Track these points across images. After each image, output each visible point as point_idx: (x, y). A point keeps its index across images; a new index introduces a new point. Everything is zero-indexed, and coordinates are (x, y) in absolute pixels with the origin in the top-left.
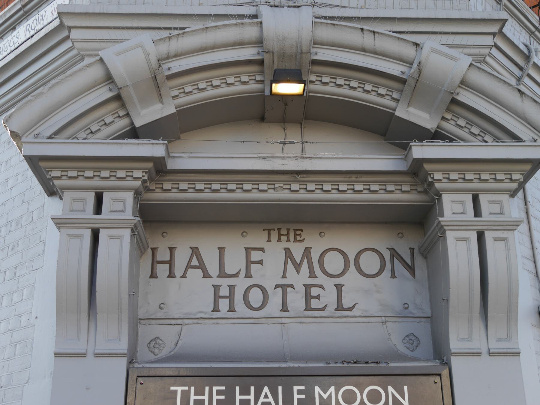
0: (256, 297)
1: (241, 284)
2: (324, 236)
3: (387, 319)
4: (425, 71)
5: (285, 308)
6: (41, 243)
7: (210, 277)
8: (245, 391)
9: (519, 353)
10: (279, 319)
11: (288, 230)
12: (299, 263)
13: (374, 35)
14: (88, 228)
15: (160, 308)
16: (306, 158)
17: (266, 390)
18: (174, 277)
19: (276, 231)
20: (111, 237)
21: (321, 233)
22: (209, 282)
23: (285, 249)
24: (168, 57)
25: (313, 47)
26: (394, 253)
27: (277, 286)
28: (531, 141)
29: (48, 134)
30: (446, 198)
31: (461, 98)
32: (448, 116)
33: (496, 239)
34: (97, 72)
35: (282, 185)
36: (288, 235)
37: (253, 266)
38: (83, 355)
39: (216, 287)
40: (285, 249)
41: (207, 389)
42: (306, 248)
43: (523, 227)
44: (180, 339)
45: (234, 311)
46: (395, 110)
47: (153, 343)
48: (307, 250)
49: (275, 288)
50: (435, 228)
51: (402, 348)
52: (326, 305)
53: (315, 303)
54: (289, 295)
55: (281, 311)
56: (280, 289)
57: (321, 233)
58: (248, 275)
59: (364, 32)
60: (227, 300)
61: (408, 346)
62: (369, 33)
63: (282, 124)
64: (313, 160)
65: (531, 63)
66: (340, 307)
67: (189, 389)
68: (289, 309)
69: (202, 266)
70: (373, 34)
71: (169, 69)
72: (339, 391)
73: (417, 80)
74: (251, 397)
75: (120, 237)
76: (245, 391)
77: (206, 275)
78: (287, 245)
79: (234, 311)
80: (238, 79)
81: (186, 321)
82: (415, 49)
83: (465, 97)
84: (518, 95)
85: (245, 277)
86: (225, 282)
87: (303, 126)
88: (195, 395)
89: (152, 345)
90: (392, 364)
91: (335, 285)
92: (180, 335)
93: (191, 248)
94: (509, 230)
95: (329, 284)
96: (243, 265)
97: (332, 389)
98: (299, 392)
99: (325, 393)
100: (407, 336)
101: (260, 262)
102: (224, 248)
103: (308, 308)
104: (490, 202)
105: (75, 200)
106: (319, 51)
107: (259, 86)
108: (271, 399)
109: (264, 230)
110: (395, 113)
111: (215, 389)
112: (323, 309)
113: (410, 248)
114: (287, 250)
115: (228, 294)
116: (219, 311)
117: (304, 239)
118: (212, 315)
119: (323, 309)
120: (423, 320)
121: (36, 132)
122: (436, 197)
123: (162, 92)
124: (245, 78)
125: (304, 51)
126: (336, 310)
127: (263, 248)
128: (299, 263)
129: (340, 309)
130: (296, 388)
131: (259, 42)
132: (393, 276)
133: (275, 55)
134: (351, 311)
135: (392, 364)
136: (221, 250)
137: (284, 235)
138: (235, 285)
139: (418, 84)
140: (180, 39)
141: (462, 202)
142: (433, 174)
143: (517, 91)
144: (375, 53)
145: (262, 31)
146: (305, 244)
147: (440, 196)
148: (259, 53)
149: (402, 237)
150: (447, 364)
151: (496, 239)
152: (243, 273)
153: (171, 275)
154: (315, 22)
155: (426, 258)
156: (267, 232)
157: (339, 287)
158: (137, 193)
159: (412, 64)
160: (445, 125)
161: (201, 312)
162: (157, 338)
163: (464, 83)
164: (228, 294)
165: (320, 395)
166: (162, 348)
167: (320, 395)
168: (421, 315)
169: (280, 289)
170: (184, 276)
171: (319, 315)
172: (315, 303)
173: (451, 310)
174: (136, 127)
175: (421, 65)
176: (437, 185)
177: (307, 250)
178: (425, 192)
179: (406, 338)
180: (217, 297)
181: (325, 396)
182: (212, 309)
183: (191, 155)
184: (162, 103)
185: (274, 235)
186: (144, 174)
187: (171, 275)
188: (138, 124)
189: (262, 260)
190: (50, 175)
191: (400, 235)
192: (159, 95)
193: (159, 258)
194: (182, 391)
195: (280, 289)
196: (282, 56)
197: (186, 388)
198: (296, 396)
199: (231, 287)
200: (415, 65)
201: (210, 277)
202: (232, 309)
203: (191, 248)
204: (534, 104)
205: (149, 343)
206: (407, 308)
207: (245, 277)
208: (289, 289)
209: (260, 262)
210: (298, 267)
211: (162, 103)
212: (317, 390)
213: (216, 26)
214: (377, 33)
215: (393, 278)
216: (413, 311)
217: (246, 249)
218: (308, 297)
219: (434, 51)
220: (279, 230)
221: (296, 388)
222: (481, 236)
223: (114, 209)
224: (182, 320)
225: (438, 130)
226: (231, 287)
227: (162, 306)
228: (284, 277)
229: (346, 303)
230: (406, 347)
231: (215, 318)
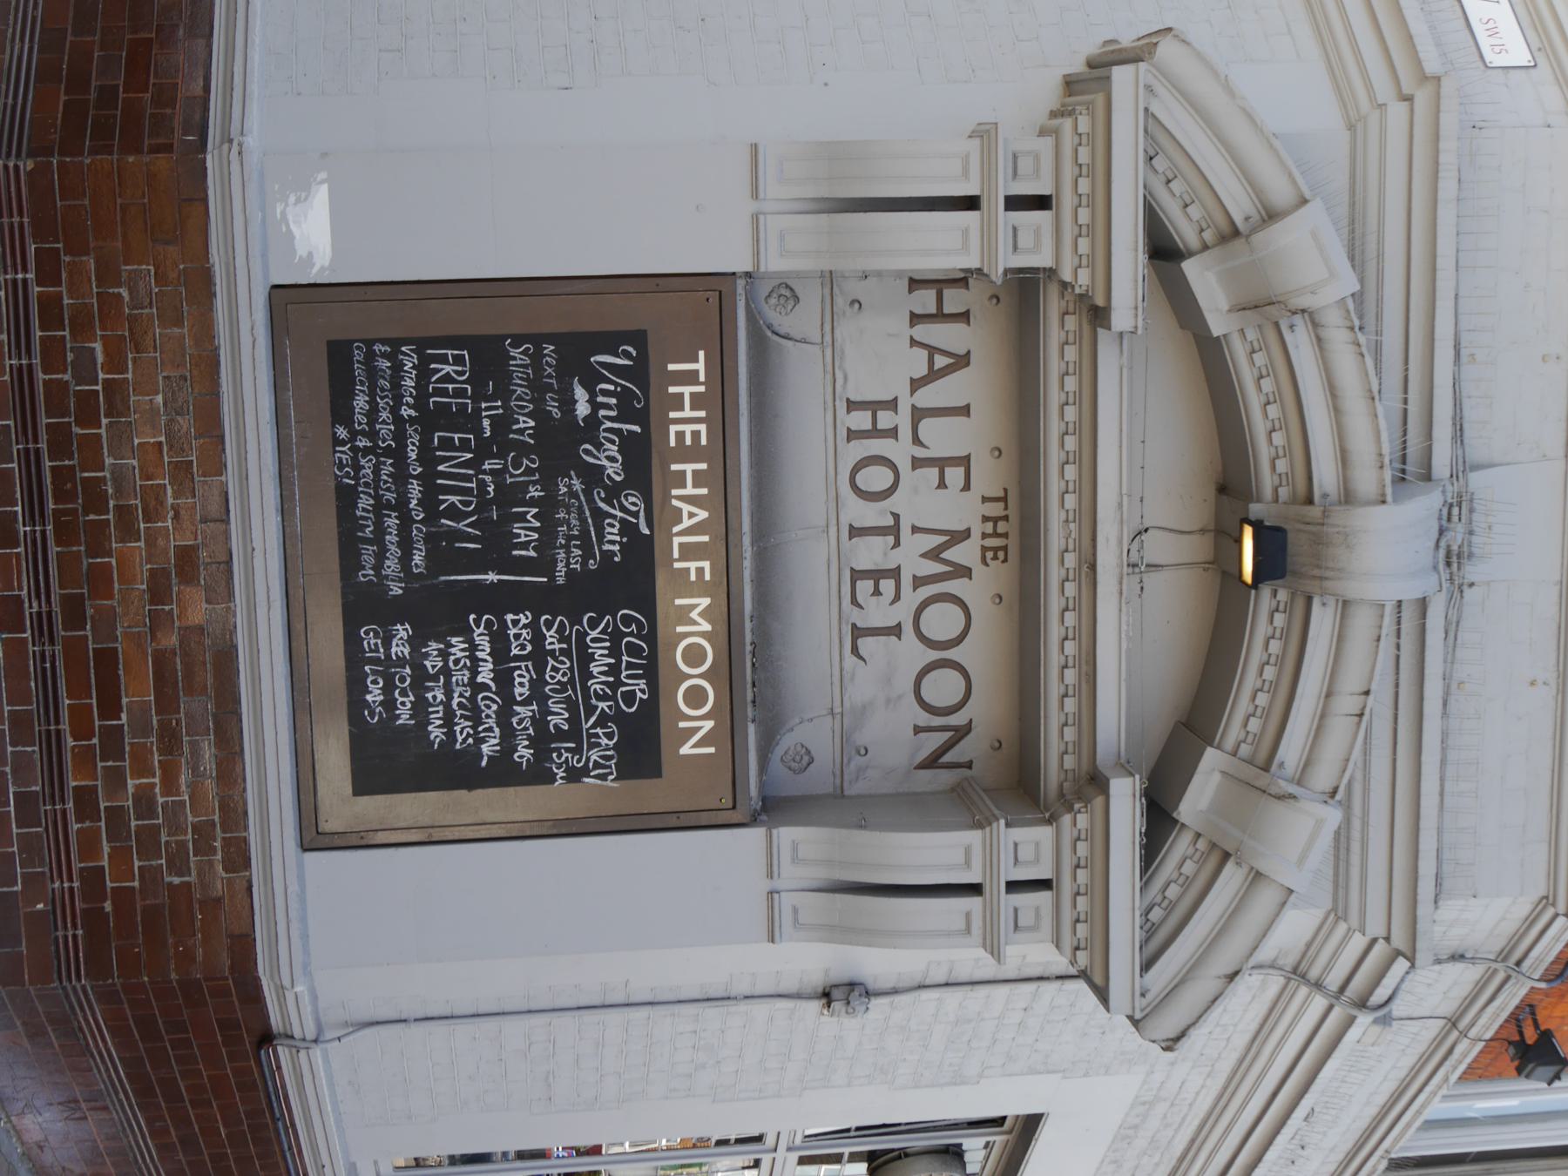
0: (876, 478)
1: (900, 451)
2: (994, 603)
4: (1279, 808)
5: (855, 532)
6: (970, 71)
7: (913, 392)
8: (699, 479)
9: (773, 941)
10: (834, 522)
11: (1005, 535)
12: (941, 556)
13: (1356, 715)
14: (983, 190)
15: (852, 302)
16: (1121, 583)
17: (703, 515)
18: (912, 325)
19: (1003, 513)
20: (966, 232)
21: (1001, 598)
22: (902, 391)
23: (968, 531)
24: (1315, 325)
25: (1337, 600)
26: (962, 732)
27: (896, 517)
28: (1141, 987)
30: (1044, 833)
31: (1230, 867)
32: (1201, 845)
33: (968, 915)
34: (1280, 193)
35: (1073, 536)
36: (996, 534)
37: (936, 471)
38: (755, 194)
39: (892, 405)
40: (968, 531)
41: (702, 414)
42: (970, 570)
43: (988, 968)
44: (797, 344)
45: (849, 440)
46: (1218, 748)
47: (788, 293)
48: (964, 572)
49: (892, 513)
50: (990, 810)
51: (787, 742)
52: (861, 607)
53: (865, 586)
54: (879, 539)
55: (851, 525)
56: (892, 523)
57: (1001, 598)
58: (917, 463)
59: (1363, 697)
60: (868, 426)
61: (791, 753)
62: (1361, 707)
64: (1117, 595)
65: (1354, 1012)
66: (858, 632)
67: (701, 384)
68: (854, 540)
69: (933, 375)
70: (1359, 712)
72: (705, 638)
73: (1264, 792)
74: (690, 490)
76: (699, 479)
77: (916, 384)
79: (849, 440)
80: (1281, 453)
82: (1327, 791)
83: (1232, 878)
85: (913, 457)
86: (903, 420)
87: (1207, 566)
88: (691, 394)
89: (784, 291)
90: (751, 728)
91: (899, 624)
93: (969, 352)
94: (985, 939)
95: (902, 613)
97: (706, 627)
98: (700, 571)
99: (700, 614)
100: (808, 752)
101: (942, 484)
102: (968, 415)
103: (857, 575)
105: (1037, 158)
107: (1268, 492)
108: (687, 523)
109: (1005, 490)
110: (1212, 746)
111: (702, 428)
112: (854, 601)
113: (971, 762)
114: (967, 534)
117: (987, 565)
118: (841, 400)
119: (854, 601)
120: (838, 781)
121: (1159, 88)
122: (1047, 815)
123: (1248, 312)
124: (1282, 466)
125: (1328, 584)
126: (854, 626)
127: (969, 489)
128: (941, 556)
129: (855, 632)
130: (706, 565)
131: (1348, 497)
132: (918, 730)
133: (1319, 527)
134: (852, 652)
135: (751, 728)
136: (965, 411)
137: (995, 527)
138: (897, 439)
139: (1259, 792)
140: (1352, 348)
141: (1037, 860)
142: (1087, 812)
143: (1237, 969)
144: (1323, 716)
145: (1369, 503)
146: (978, 569)
147: (1049, 822)
148: (1325, 496)
149: (993, 748)
150: (752, 821)
151: (968, 915)
152: (920, 453)
153: (915, 318)
154: (1384, 605)
155: (953, 790)
156: (1001, 494)
157: (896, 631)
158: (1051, 273)
159: (1299, 783)
162: (797, 299)
166: (778, 310)
168: (846, 777)
169: (890, 522)
170: (914, 342)
171: (843, 593)
172: (865, 586)
173: (844, 832)
174: (1182, 261)
175: (1292, 801)
177: (964, 572)
178: (1061, 795)
179: (804, 750)
180: (874, 406)
181: (694, 615)
182: (852, 399)
183: (1125, 371)
184: (1230, 311)
185: (996, 509)
186: (1084, 288)
187: (915, 318)
189: (946, 487)
190: (1081, 114)
191: (997, 745)
192: (1243, 306)
193: (948, 293)
194: (697, 372)
195: (890, 522)
197: (702, 378)
198: (693, 566)
199: (893, 433)
201: (913, 392)
202: (852, 435)
203: (969, 352)
204: (1211, 998)
205: (787, 286)
207: (913, 457)
208: (891, 539)
209: (942, 484)
210: (934, 554)
213: (1376, 416)
214: (1360, 721)
215: (914, 729)
216: (853, 764)
217: (968, 457)
218: (877, 575)
219: (1319, 823)
220: (1006, 518)
221: (706, 565)
222: (974, 889)
223: (1020, 234)
224: (830, 343)
225: (1178, 826)
226: (893, 433)
227: (857, 306)
228: (915, 529)
229: (865, 644)
230: (789, 749)
231: (834, 406)
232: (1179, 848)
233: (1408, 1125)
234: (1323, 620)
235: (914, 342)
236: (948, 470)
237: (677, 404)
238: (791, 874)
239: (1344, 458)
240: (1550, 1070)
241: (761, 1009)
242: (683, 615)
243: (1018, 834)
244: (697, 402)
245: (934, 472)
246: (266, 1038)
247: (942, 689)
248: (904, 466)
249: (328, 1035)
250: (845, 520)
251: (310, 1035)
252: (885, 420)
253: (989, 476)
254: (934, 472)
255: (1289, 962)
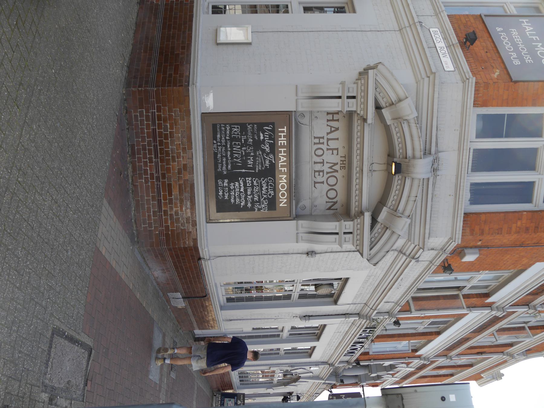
0: (319, 152)
1: (324, 147)
3: (311, 200)
5: (315, 163)
7: (327, 135)
8: (284, 152)
11: (345, 164)
15: (315, 117)
17: (285, 159)
18: (327, 122)
20: (338, 103)
26: (335, 203)
27: (323, 160)
29: (377, 79)
31: (388, 230)
32: (382, 226)
33: (336, 239)
34: (402, 95)
36: (343, 164)
37: (331, 151)
38: (297, 95)
39: (323, 138)
41: (285, 139)
43: (339, 249)
47: (303, 115)
48: (337, 171)
51: (301, 204)
53: (317, 174)
54: (320, 164)
58: (328, 149)
63: (386, 163)
66: (315, 183)
69: (331, 132)
71: (404, 123)
75: (338, 106)
76: (284, 152)
77: (328, 134)
78: (339, 164)
81: (311, 127)
83: (388, 232)
84: (387, 250)
92: (306, 125)
95: (324, 179)
96: (331, 147)
97: (285, 181)
98: (284, 170)
99: (284, 179)
100: (305, 206)
101: (333, 154)
103: (315, 171)
104: (349, 238)
106: (410, 180)
108: (282, 160)
114: (337, 164)
115: (320, 142)
116: (314, 139)
121: (378, 74)
125: (409, 175)
130: (286, 169)
131: (414, 157)
136: (338, 139)
140: (416, 127)
144: (407, 201)
145: (418, 159)
146: (339, 171)
147: (352, 221)
148: (409, 157)
152: (329, 147)
153: (328, 120)
155: (333, 214)
156: (344, 156)
157: (323, 183)
159: (402, 214)
160: (379, 224)
161: (314, 132)
162: (304, 116)
163: (393, 232)
164: (320, 142)
165: (283, 177)
167: (283, 177)
169: (322, 161)
170: (328, 125)
173: (312, 222)
176: (356, 220)
177: (337, 171)
178: (355, 215)
180: (319, 138)
181: (283, 179)
187: (328, 120)
188: (383, 111)
193: (335, 115)
195: (322, 161)
196: (408, 166)
197: (285, 132)
200: (401, 215)
201: (327, 135)
202: (315, 144)
206: (315, 206)
208: (322, 164)
209: (333, 154)
210: (331, 168)
211: (391, 120)
212: (285, 176)
217: (338, 148)
219: (406, 222)
220: (345, 161)
221: (286, 169)
222: (337, 234)
226: (323, 143)
228: (327, 163)
229: (317, 185)
232: (378, 227)
233: (421, 282)
234: (408, 182)
235: (328, 125)
236: (334, 151)
237: (280, 137)
238: (301, 230)
239: (413, 149)
240: (450, 272)
241: (295, 256)
242: (281, 179)
243: (346, 223)
244: (284, 136)
245: (331, 151)
246: (200, 259)
247: (332, 194)
248: (325, 150)
249: (211, 258)
250: (313, 160)
251: (208, 258)
252: (321, 141)
253: (342, 152)
254: (331, 151)
255: (399, 249)
